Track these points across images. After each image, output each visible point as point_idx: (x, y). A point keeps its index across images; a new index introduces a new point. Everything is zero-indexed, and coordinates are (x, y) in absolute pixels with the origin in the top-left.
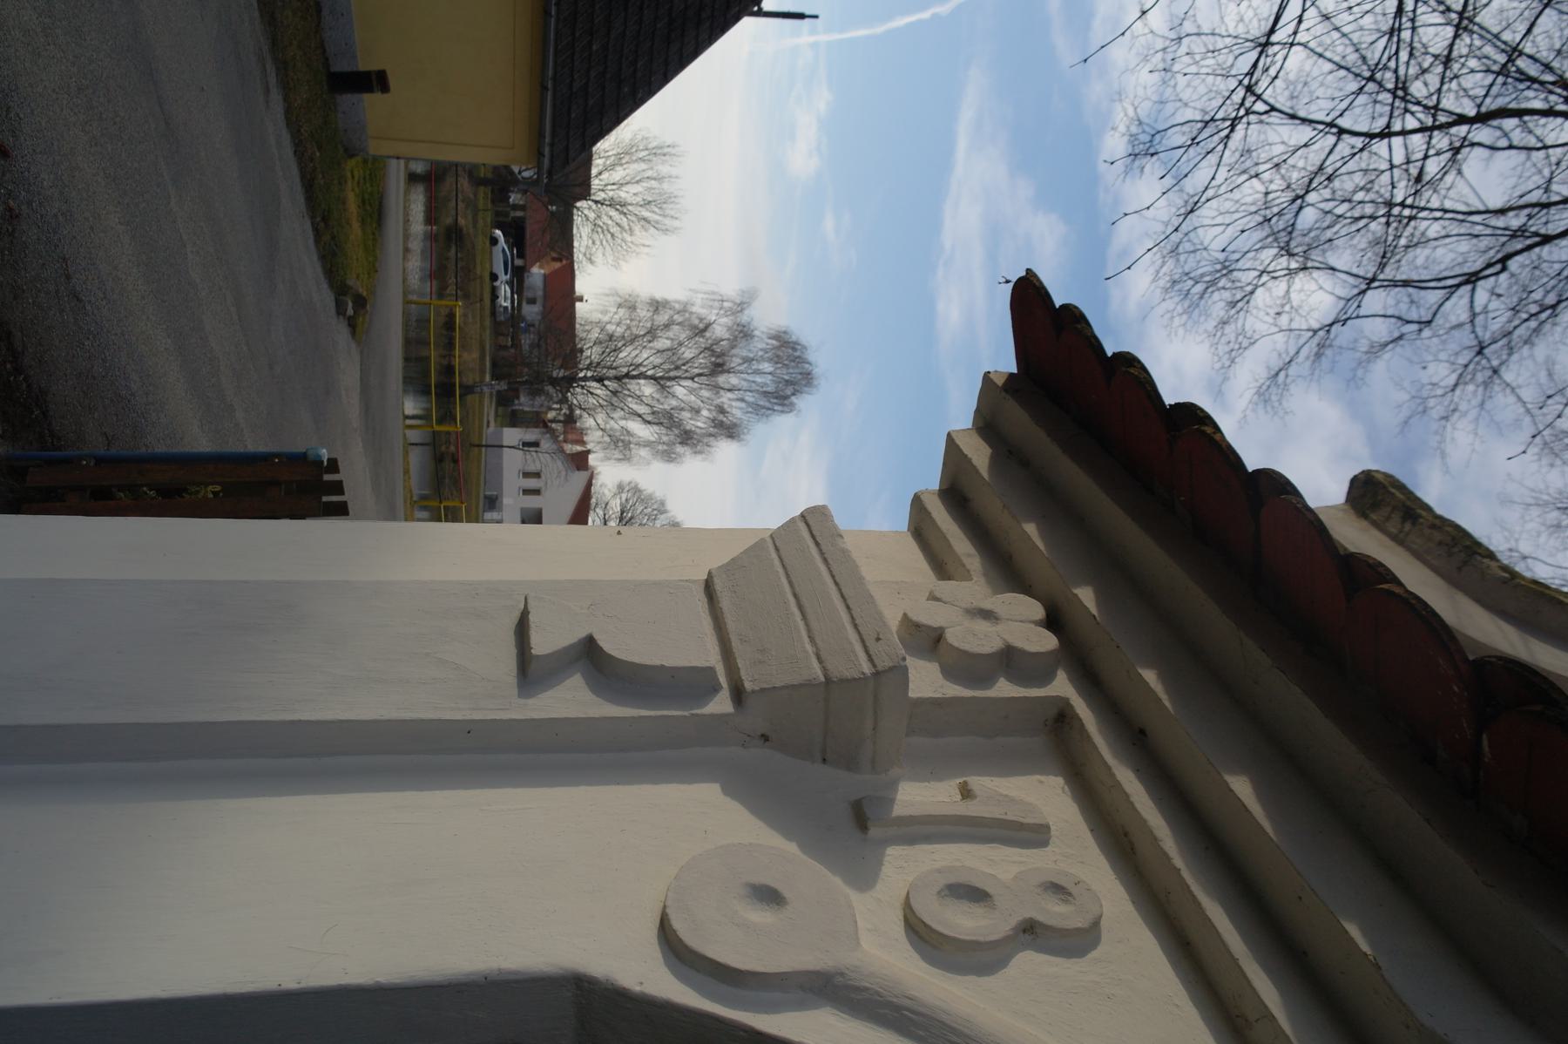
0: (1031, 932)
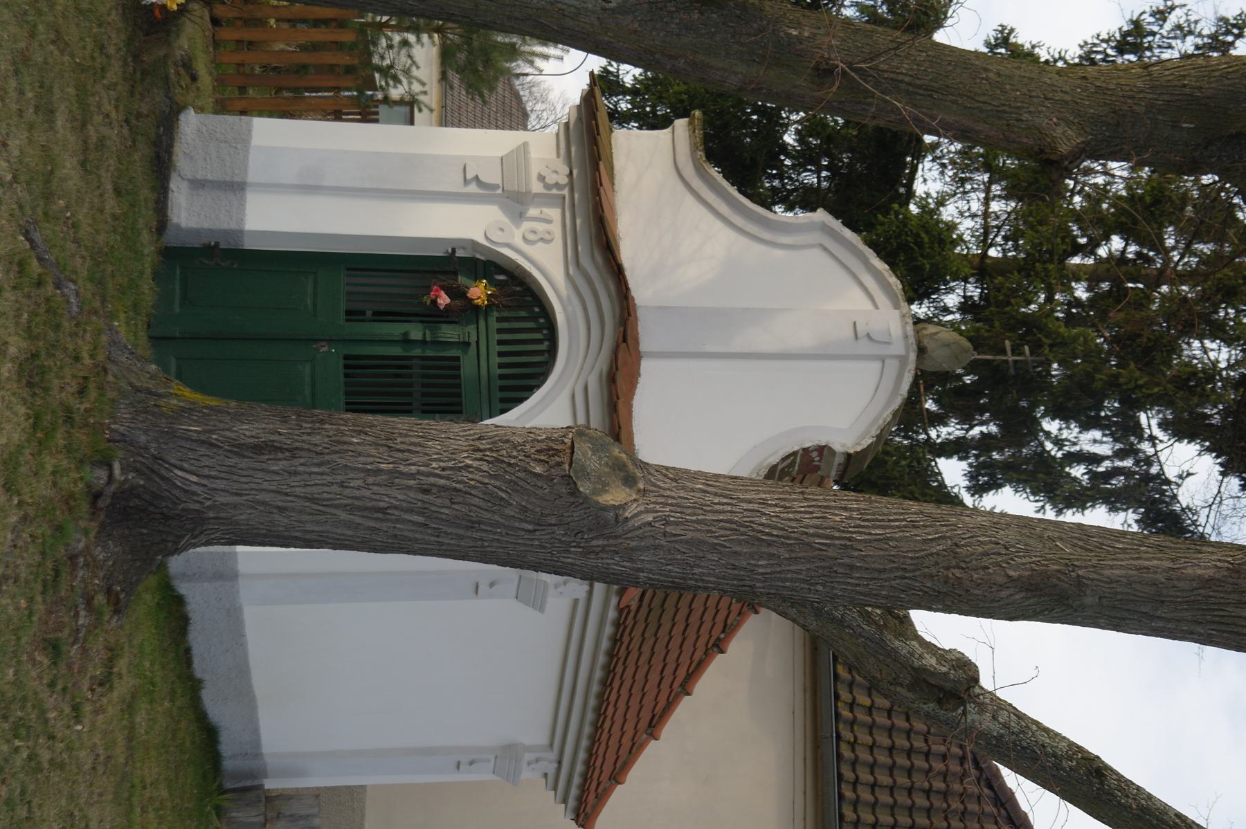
0: (542, 239)
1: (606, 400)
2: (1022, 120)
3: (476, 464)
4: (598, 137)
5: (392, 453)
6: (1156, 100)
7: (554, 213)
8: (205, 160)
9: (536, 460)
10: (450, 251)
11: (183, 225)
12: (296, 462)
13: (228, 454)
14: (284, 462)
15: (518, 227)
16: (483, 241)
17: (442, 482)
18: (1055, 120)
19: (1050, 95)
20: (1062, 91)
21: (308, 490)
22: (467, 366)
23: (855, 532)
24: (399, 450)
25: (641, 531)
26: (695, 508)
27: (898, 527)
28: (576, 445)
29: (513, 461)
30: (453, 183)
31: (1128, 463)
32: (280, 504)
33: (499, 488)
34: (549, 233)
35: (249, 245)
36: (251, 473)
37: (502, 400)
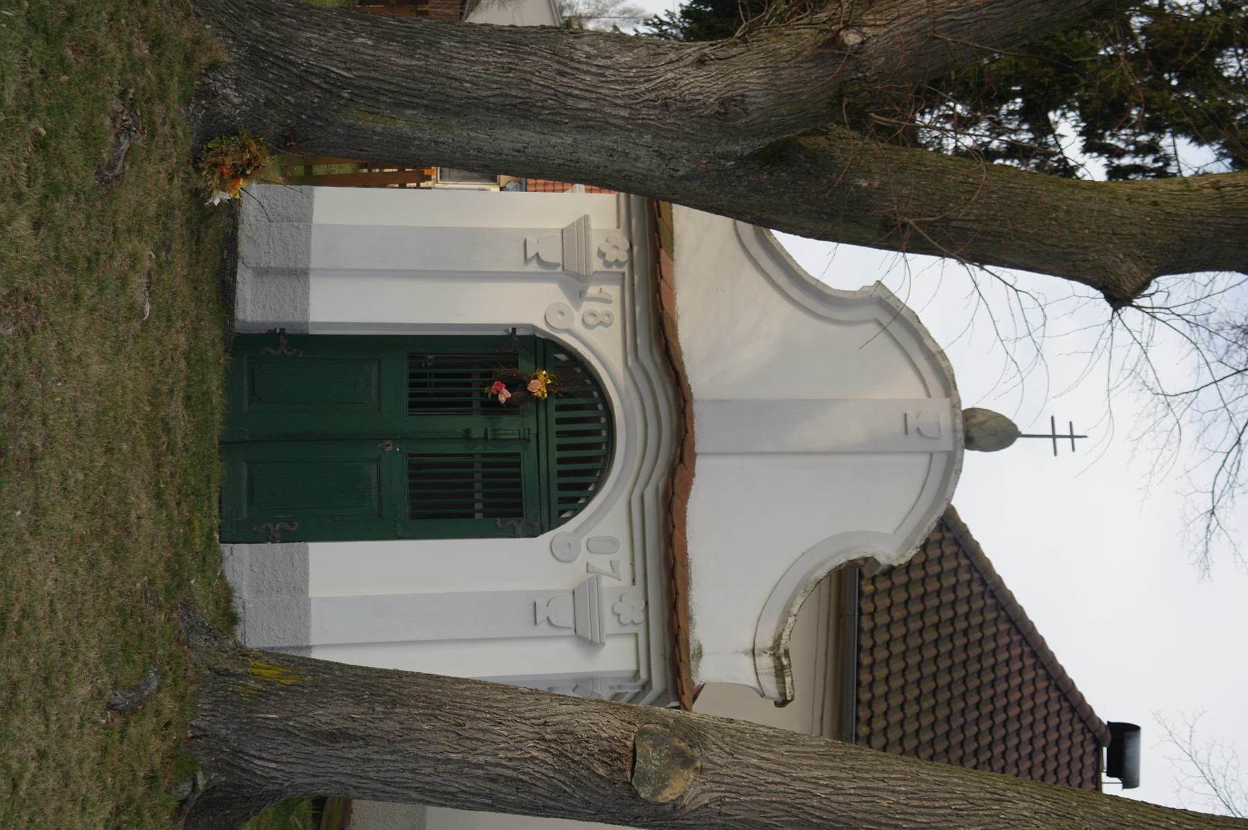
0: (601, 323)
1: (661, 524)
2: (1088, 260)
3: (541, 755)
4: (659, 220)
5: (461, 742)
6: (1225, 224)
7: (613, 291)
8: (268, 243)
9: (599, 760)
10: (510, 331)
11: (249, 319)
12: (370, 750)
13: (307, 743)
14: (358, 750)
15: (578, 308)
16: (542, 326)
17: (509, 773)
18: (1121, 256)
19: (1118, 230)
20: (1131, 223)
21: (382, 775)
22: (528, 468)
23: (901, 819)
24: (467, 738)
25: (697, 813)
26: (749, 787)
27: (943, 815)
28: (639, 750)
29: (577, 758)
30: (513, 261)
31: (1149, 160)
32: (354, 784)
33: (563, 782)
34: (608, 315)
35: (312, 332)
36: (327, 759)
37: (562, 500)
